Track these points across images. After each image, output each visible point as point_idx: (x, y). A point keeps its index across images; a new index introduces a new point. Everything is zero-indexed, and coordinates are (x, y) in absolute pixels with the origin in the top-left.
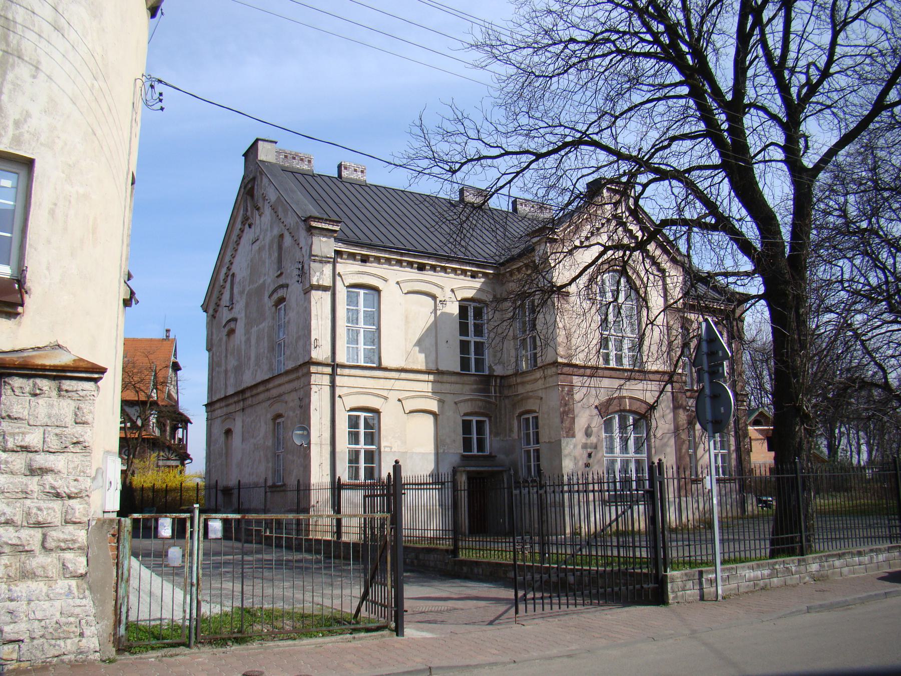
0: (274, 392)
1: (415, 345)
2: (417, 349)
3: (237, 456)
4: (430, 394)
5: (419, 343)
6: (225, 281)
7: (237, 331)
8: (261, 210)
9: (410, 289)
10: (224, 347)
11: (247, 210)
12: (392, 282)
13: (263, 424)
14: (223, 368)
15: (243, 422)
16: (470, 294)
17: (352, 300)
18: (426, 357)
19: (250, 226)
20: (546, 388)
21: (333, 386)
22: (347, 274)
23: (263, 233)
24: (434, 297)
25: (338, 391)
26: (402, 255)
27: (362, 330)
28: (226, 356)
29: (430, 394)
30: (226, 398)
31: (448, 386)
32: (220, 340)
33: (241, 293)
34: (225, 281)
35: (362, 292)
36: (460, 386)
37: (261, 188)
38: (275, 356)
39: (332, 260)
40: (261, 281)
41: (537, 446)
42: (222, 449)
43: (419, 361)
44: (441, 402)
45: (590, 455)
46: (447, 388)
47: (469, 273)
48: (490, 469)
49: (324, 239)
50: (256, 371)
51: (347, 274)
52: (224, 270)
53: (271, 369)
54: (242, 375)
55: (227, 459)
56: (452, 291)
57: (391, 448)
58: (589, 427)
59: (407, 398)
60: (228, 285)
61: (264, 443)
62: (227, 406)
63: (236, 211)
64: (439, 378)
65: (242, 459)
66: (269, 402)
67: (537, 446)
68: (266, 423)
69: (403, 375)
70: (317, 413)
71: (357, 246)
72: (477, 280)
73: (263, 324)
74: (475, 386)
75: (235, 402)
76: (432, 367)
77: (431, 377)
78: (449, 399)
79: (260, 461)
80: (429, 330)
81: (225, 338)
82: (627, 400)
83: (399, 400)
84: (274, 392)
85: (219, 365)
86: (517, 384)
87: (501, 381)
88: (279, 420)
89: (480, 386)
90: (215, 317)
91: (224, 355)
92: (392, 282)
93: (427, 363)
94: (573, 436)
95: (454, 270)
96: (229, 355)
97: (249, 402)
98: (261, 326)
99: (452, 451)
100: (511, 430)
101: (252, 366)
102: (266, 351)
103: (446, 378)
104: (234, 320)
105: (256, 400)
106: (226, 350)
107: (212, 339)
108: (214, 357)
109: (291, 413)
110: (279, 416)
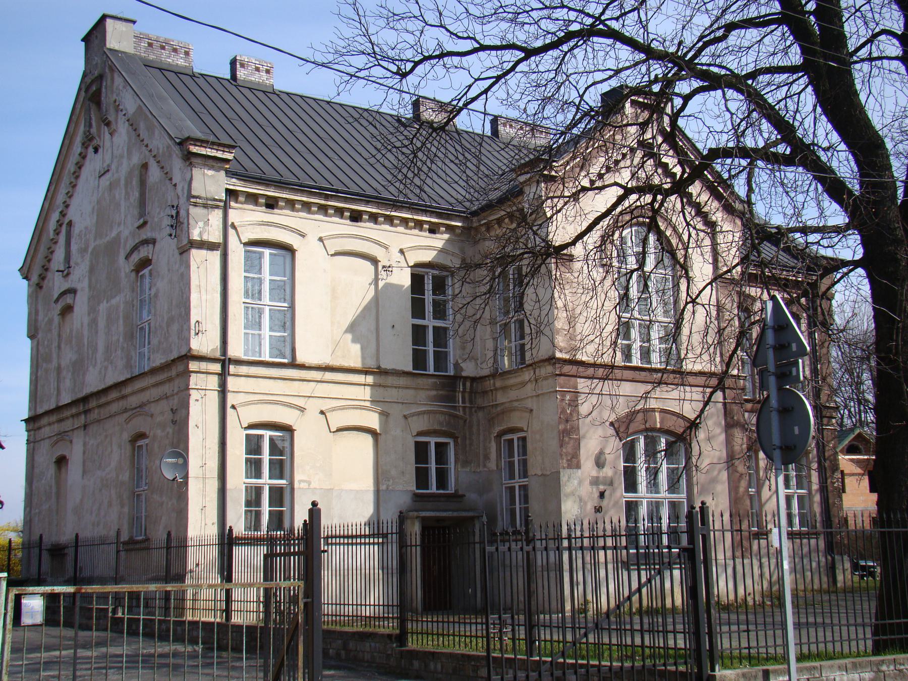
0: (134, 401)
1: (346, 331)
2: (349, 336)
3: (74, 496)
4: (368, 404)
5: (352, 328)
6: (57, 232)
7: (76, 309)
8: (113, 126)
9: (339, 249)
10: (55, 332)
11: (90, 126)
12: (312, 239)
13: (115, 448)
14: (55, 363)
15: (85, 444)
16: (428, 256)
17: (252, 264)
18: (362, 349)
19: (96, 150)
20: (538, 396)
21: (223, 391)
22: (244, 226)
23: (115, 160)
24: (374, 261)
25: (231, 399)
26: (327, 197)
27: (267, 309)
28: (59, 347)
29: (368, 404)
30: (58, 409)
31: (394, 392)
32: (50, 321)
33: (83, 251)
34: (57, 232)
35: (267, 252)
36: (411, 392)
37: (112, 92)
38: (135, 347)
39: (222, 204)
40: (114, 234)
41: (524, 481)
42: (51, 487)
43: (353, 356)
44: (384, 415)
45: (602, 495)
46: (392, 395)
47: (262, 201)
48: (455, 514)
49: (210, 173)
50: (106, 368)
51: (244, 226)
52: (55, 216)
53: (129, 365)
54: (84, 374)
55: (58, 502)
56: (402, 252)
57: (309, 483)
58: (601, 453)
59: (333, 409)
60: (62, 239)
61: (118, 476)
62: (60, 421)
63: (73, 125)
64: (382, 380)
65: (82, 500)
66: (126, 415)
67: (524, 481)
68: (120, 447)
69: (329, 376)
70: (199, 432)
71: (259, 184)
72: (438, 236)
73: (118, 298)
74: (434, 393)
75: (73, 416)
76: (371, 364)
77: (370, 379)
78: (396, 411)
79: (110, 505)
80: (367, 308)
81: (57, 319)
82: (657, 414)
83: (322, 412)
84: (134, 401)
85: (48, 359)
86: (496, 389)
87: (471, 386)
88: (141, 443)
89: (441, 392)
90: (41, 287)
91: (55, 344)
92: (312, 239)
93: (363, 358)
94: (578, 466)
95: (405, 222)
96: (63, 346)
97: (94, 415)
98: (114, 301)
99: (400, 487)
100: (487, 457)
101: (99, 361)
102: (121, 339)
103: (390, 380)
104: (72, 291)
105: (105, 412)
106: (59, 336)
107: (36, 320)
108: (40, 348)
109: (159, 432)
110: (142, 436)
